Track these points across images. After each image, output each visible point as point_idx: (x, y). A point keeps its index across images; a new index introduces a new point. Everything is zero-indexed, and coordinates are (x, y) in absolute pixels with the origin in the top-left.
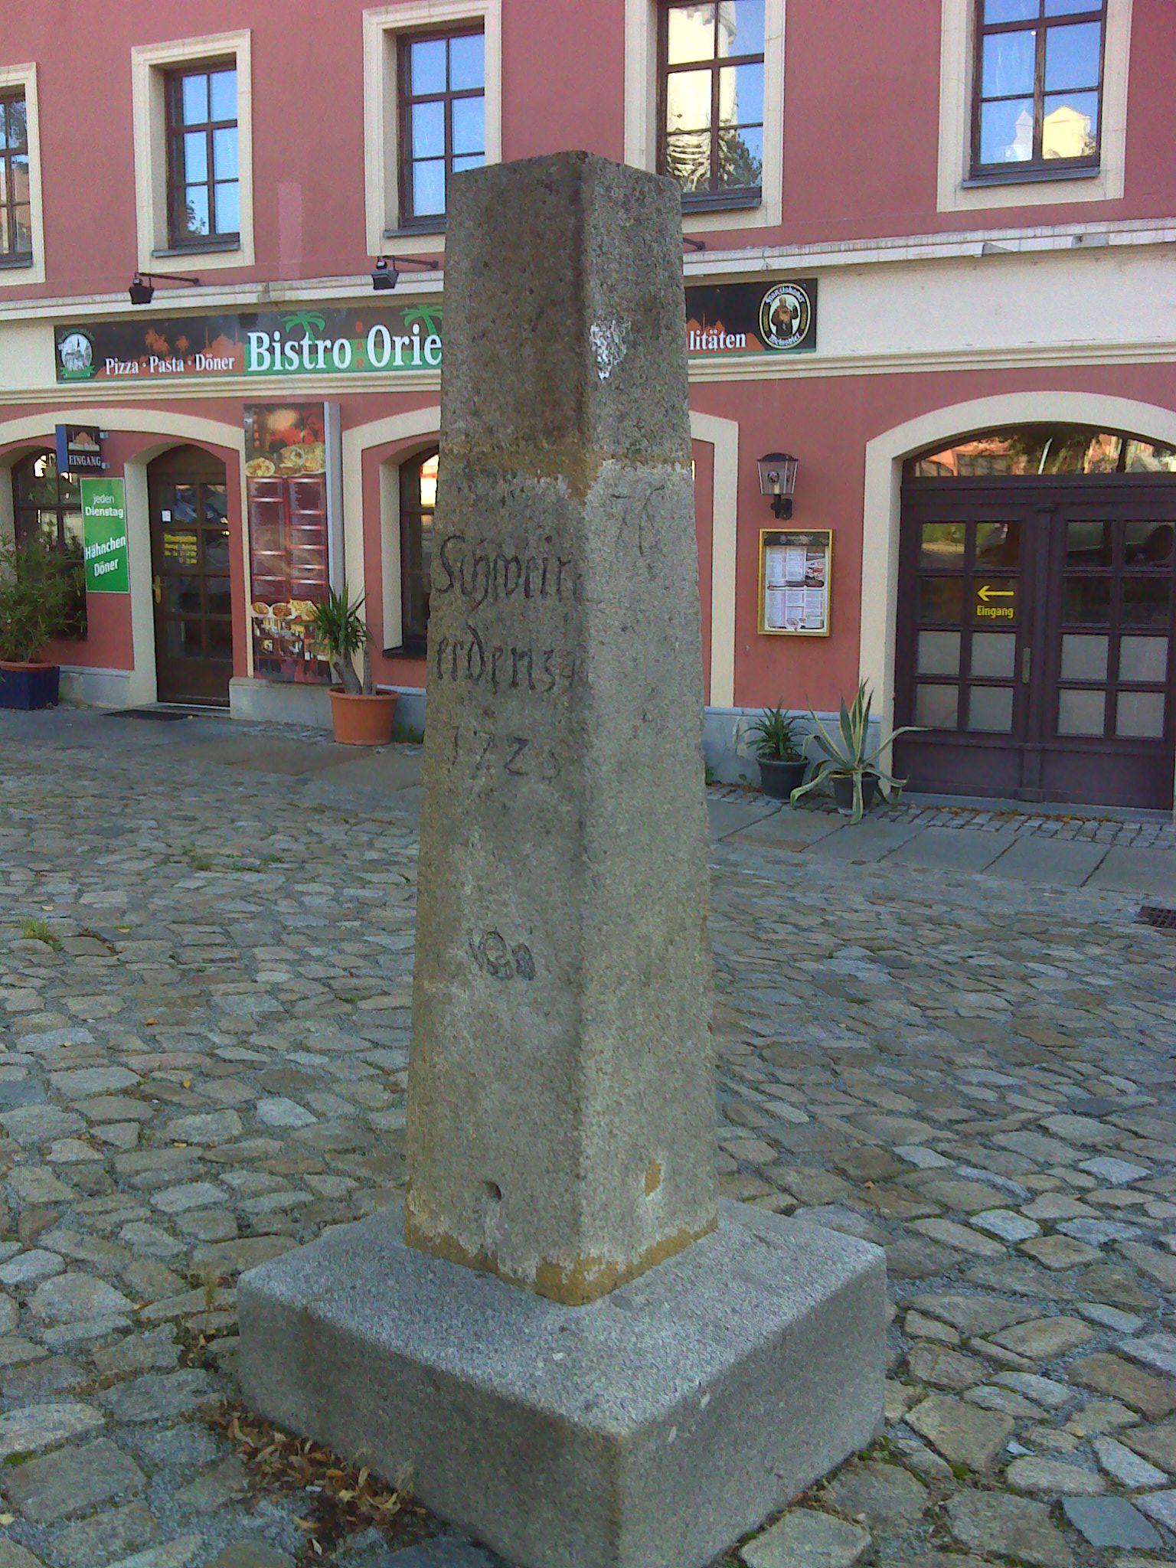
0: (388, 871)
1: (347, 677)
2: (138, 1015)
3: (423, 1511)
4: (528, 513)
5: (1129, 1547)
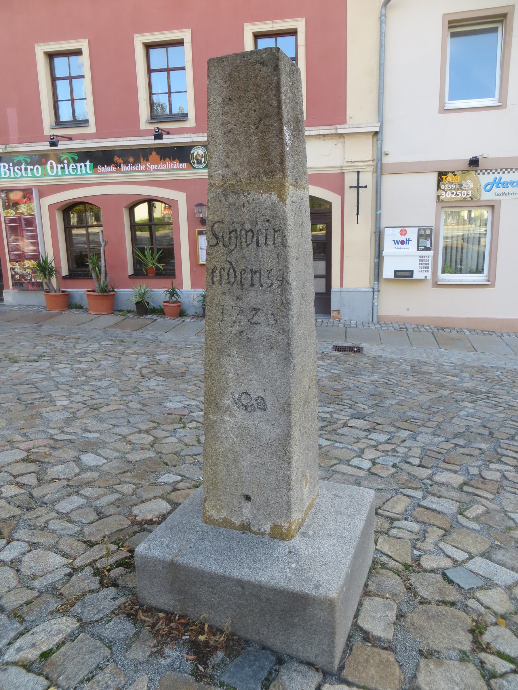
0: (86, 356)
1: (50, 287)
2: (15, 425)
3: (236, 637)
4: (257, 210)
5: (475, 587)
